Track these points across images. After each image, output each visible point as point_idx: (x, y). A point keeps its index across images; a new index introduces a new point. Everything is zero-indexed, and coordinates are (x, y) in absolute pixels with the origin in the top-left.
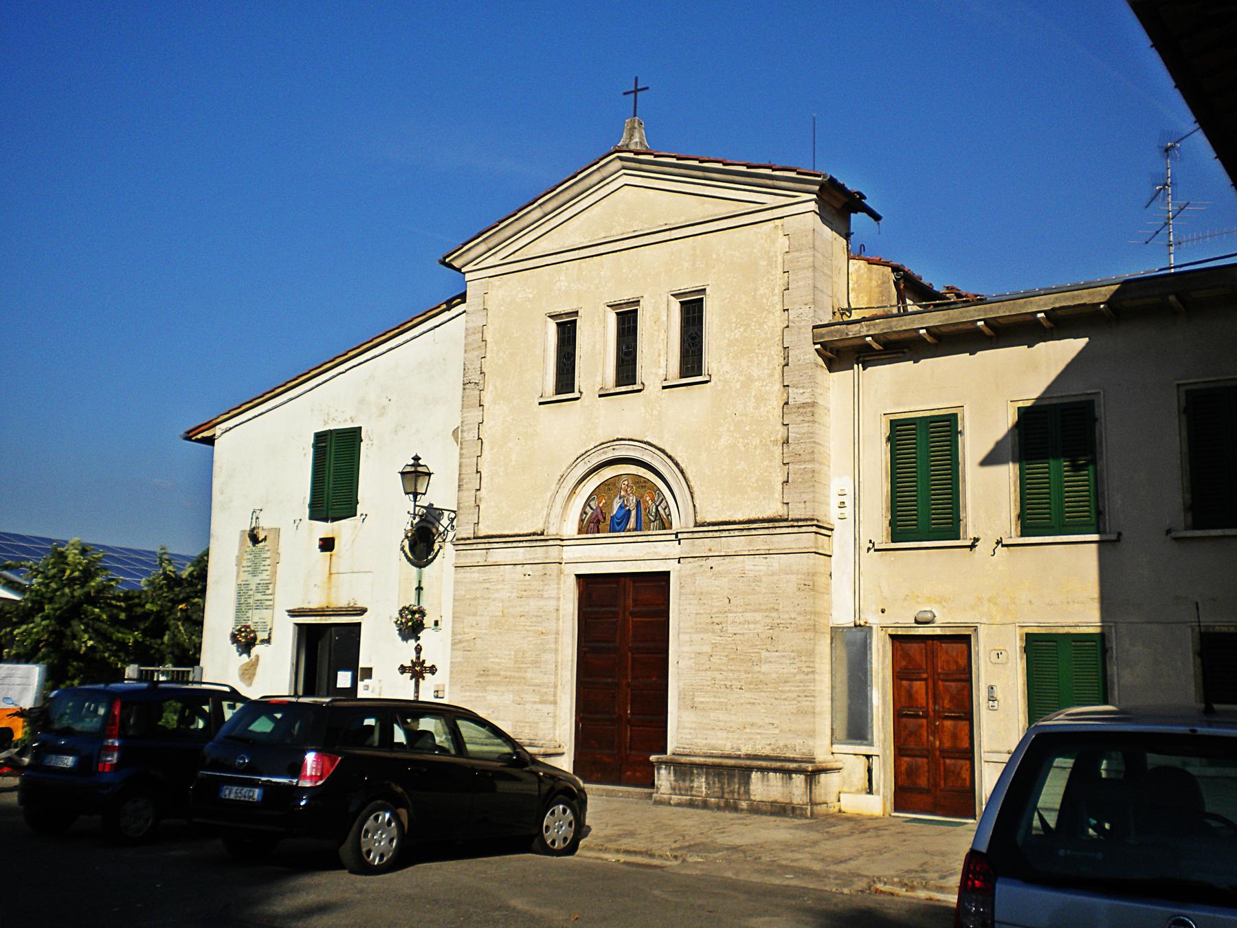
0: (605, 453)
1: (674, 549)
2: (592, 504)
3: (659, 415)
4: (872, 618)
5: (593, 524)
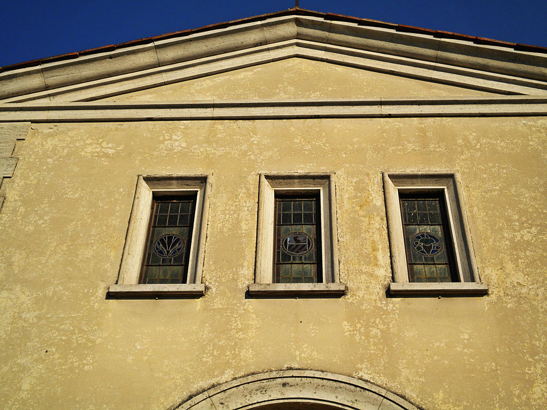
0: (263, 390)
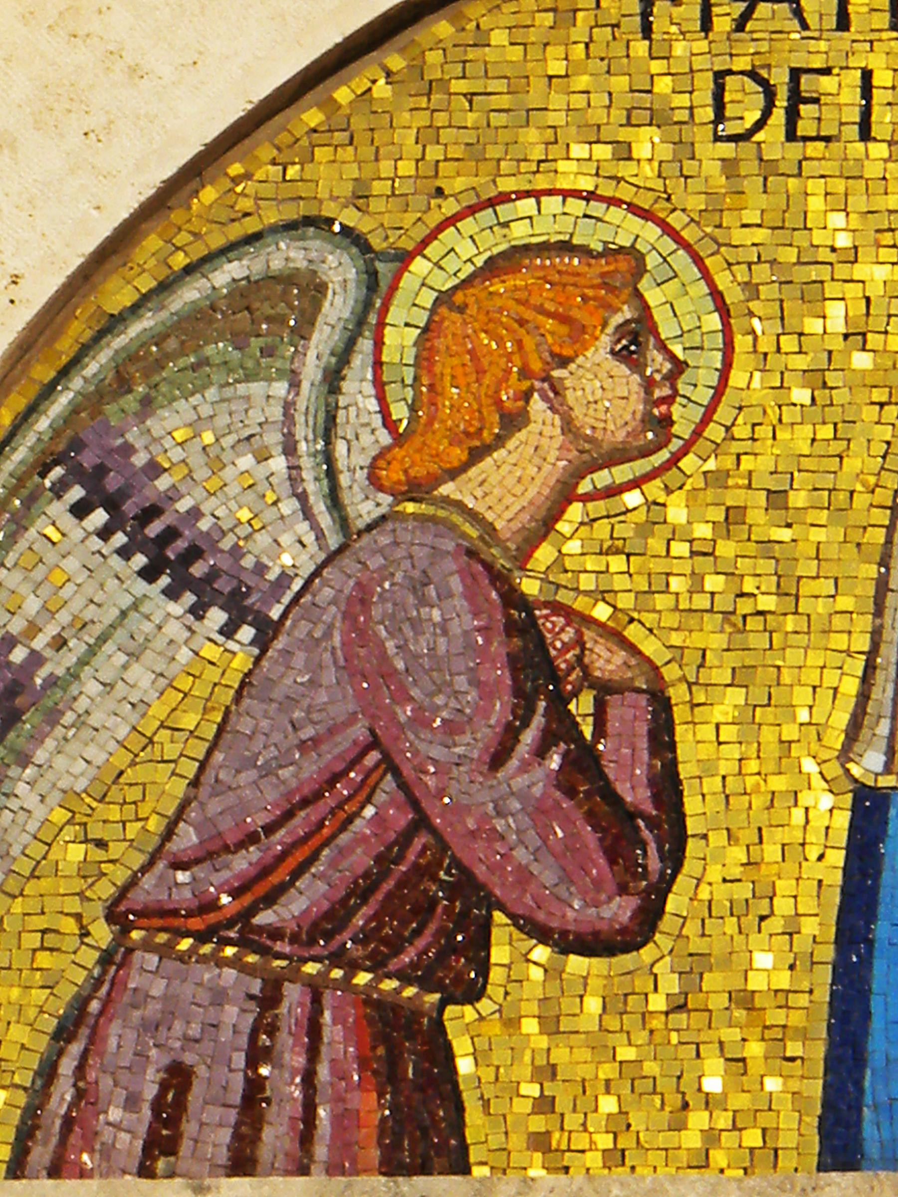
2: (228, 458)
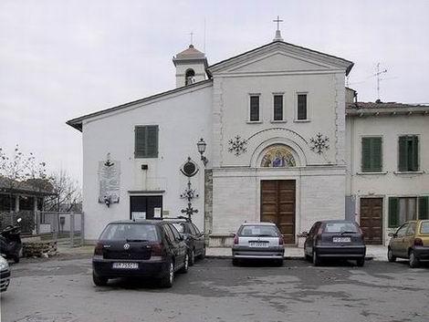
1: (297, 173)
3: (292, 132)
4: (355, 192)
5: (267, 164)
